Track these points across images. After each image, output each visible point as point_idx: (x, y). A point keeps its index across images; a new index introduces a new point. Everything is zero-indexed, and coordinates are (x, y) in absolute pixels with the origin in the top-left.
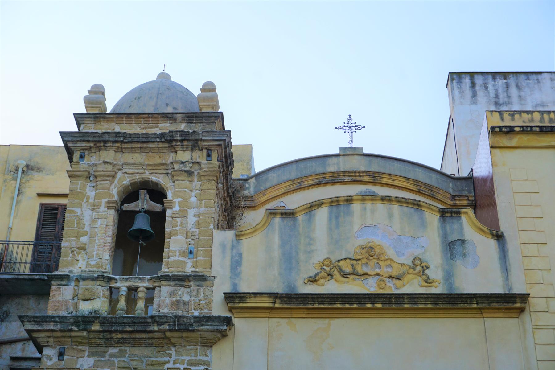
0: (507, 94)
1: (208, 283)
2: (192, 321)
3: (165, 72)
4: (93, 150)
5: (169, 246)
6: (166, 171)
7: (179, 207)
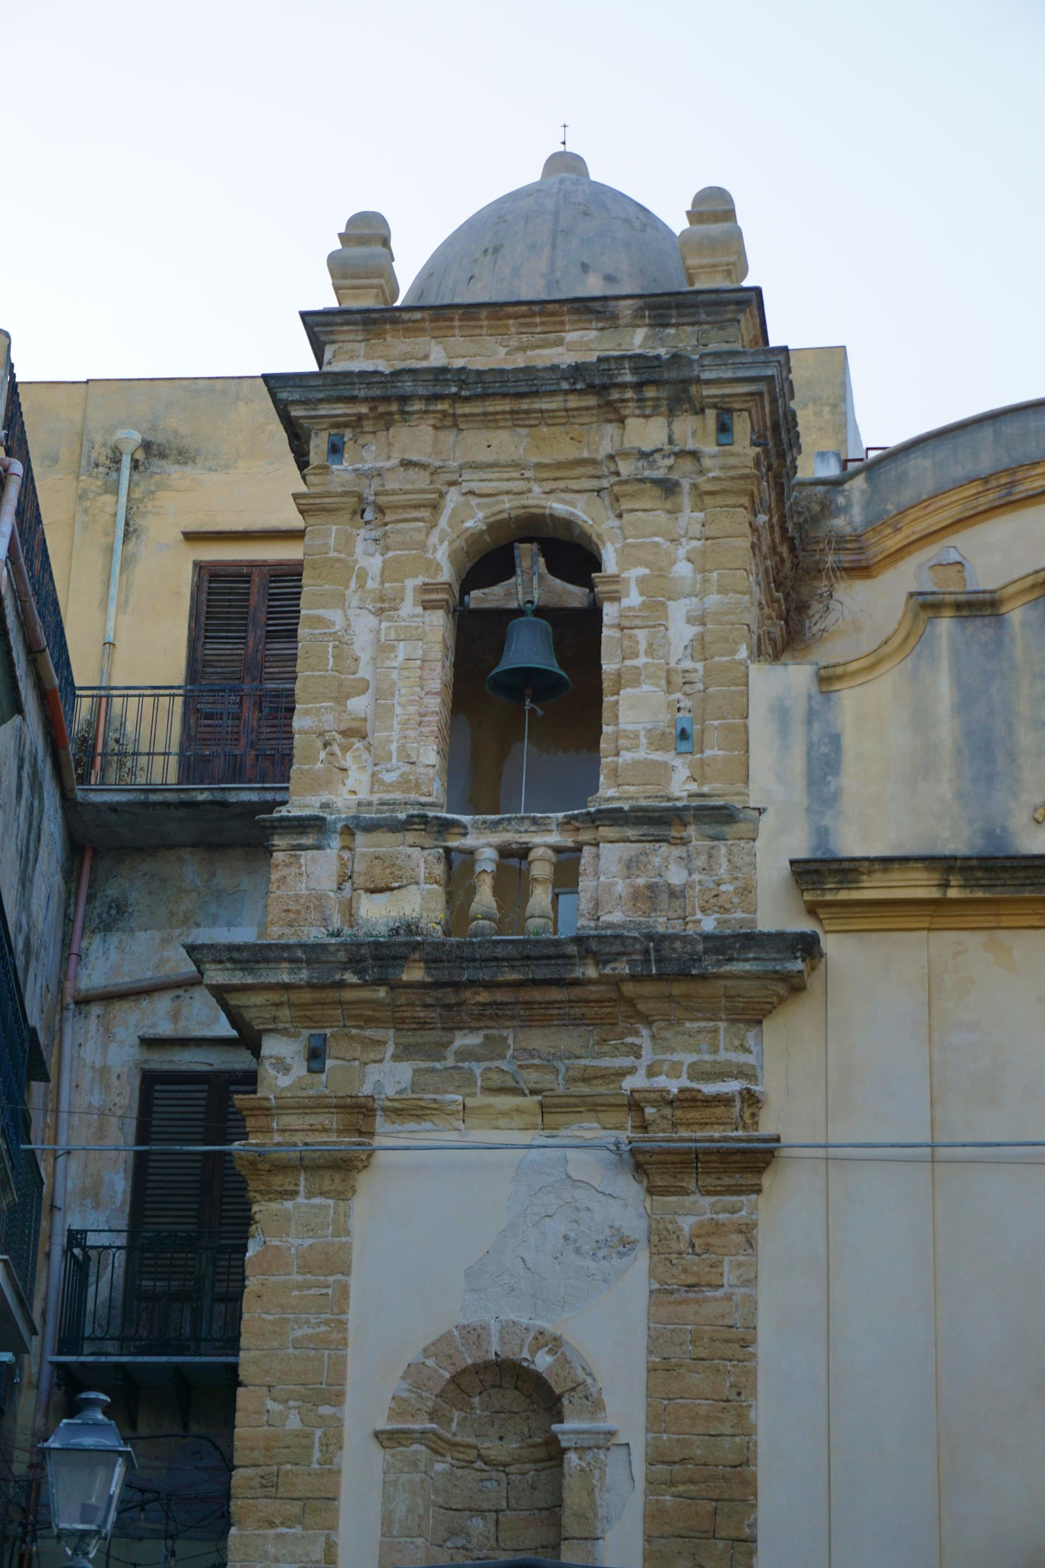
2: (700, 948)
6: (595, 484)
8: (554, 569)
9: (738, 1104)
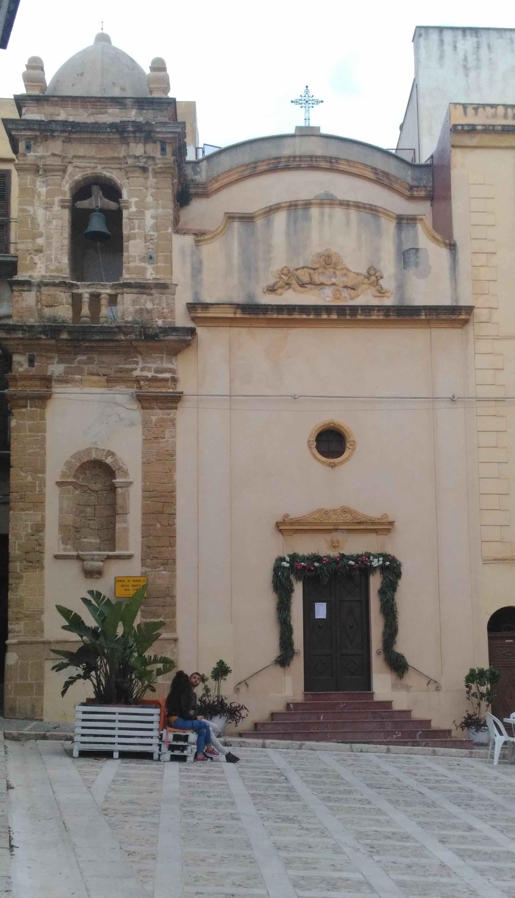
0: (477, 56)
1: (170, 291)
3: (104, 32)
5: (128, 250)
6: (119, 166)
7: (136, 207)
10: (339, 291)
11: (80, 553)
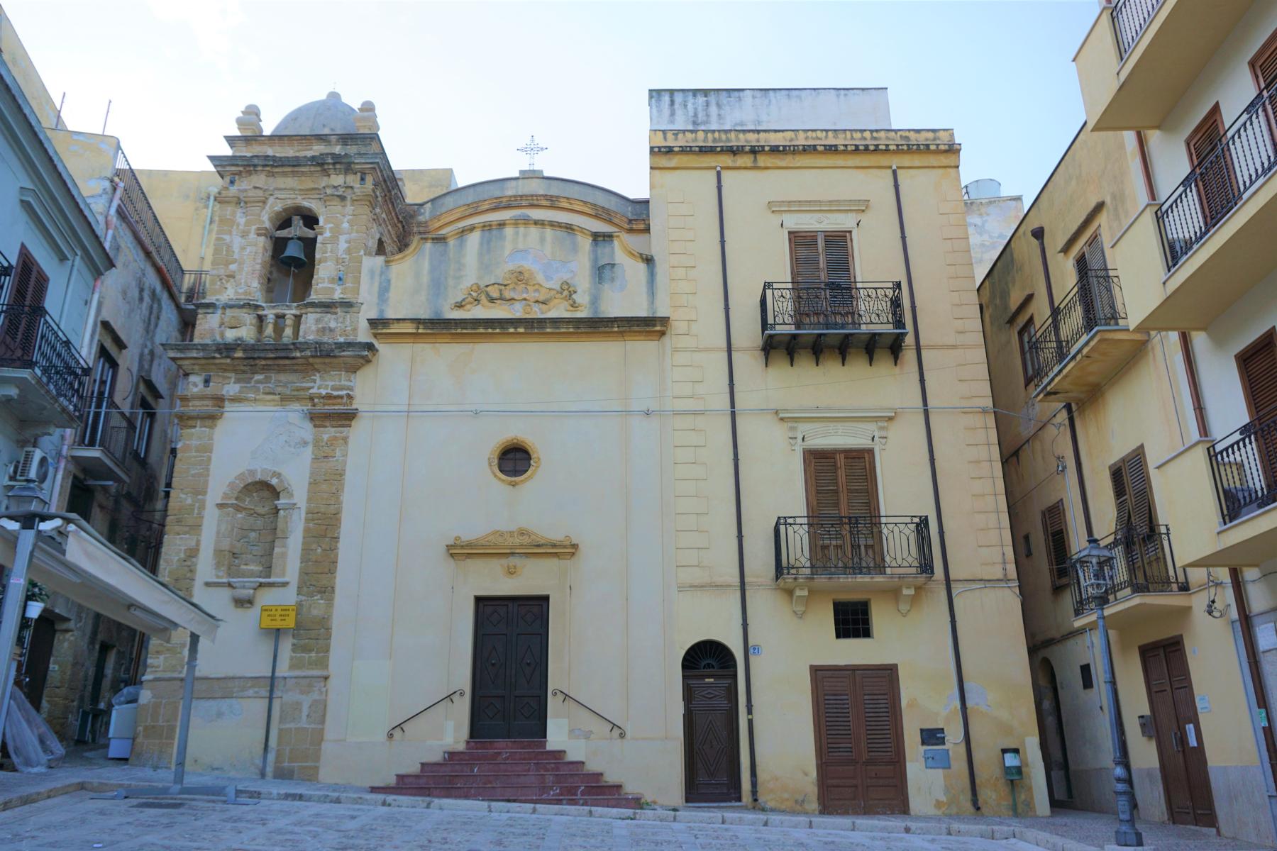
2: (333, 347)
4: (244, 175)
6: (318, 196)
8: (306, 225)
9: (345, 398)
10: (529, 305)
11: (231, 580)
